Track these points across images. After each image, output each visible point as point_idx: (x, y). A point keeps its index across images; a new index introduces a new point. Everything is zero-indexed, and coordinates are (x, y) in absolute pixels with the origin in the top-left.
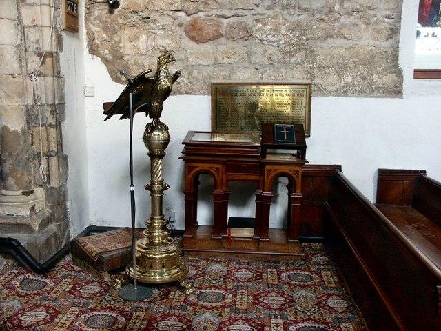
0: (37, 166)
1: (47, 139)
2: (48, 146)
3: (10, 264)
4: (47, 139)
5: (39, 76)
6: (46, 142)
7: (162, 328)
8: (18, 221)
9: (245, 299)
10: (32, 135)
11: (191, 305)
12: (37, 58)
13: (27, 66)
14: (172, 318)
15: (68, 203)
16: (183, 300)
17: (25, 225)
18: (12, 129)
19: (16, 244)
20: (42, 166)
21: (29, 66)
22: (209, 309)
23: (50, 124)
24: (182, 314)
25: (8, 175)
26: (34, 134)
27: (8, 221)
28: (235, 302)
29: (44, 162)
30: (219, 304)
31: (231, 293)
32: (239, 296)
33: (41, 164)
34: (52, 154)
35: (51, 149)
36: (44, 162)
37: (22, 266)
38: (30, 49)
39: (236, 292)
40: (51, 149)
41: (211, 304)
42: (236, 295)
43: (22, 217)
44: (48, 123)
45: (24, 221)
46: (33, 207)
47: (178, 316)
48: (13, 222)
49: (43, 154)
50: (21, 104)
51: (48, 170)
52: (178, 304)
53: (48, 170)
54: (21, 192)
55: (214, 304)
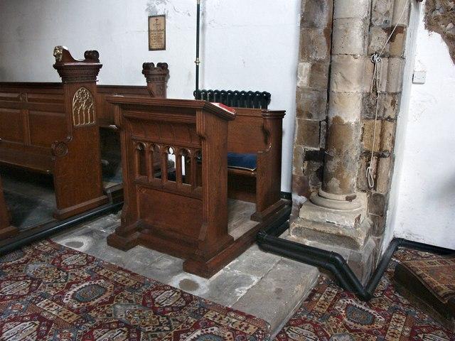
0: (364, 166)
1: (382, 136)
2: (381, 144)
3: (324, 279)
4: (382, 136)
5: (383, 56)
6: (379, 139)
7: (292, 335)
8: (341, 232)
9: (400, 330)
10: (363, 129)
11: (334, 316)
12: (384, 35)
13: (369, 44)
14: (307, 326)
15: (388, 212)
16: (327, 307)
17: (349, 238)
18: (346, 121)
19: (341, 262)
20: (370, 168)
21: (372, 44)
22: (351, 331)
23: (389, 117)
24: (321, 323)
25: (331, 175)
26: (366, 128)
27: (328, 230)
28: (386, 329)
29: (373, 162)
30: (365, 327)
31: (384, 316)
32: (393, 323)
33: (369, 165)
34: (385, 154)
35: (384, 149)
36: (373, 162)
37: (341, 286)
38: (377, 24)
39: (391, 316)
40: (384, 149)
41: (356, 325)
42: (389, 321)
43: (345, 227)
44: (386, 116)
45: (348, 233)
46: (359, 218)
47: (315, 325)
48: (334, 232)
49: (374, 152)
50: (359, 91)
51: (376, 173)
52: (321, 310)
53: (376, 173)
54: (345, 196)
55: (359, 327)
